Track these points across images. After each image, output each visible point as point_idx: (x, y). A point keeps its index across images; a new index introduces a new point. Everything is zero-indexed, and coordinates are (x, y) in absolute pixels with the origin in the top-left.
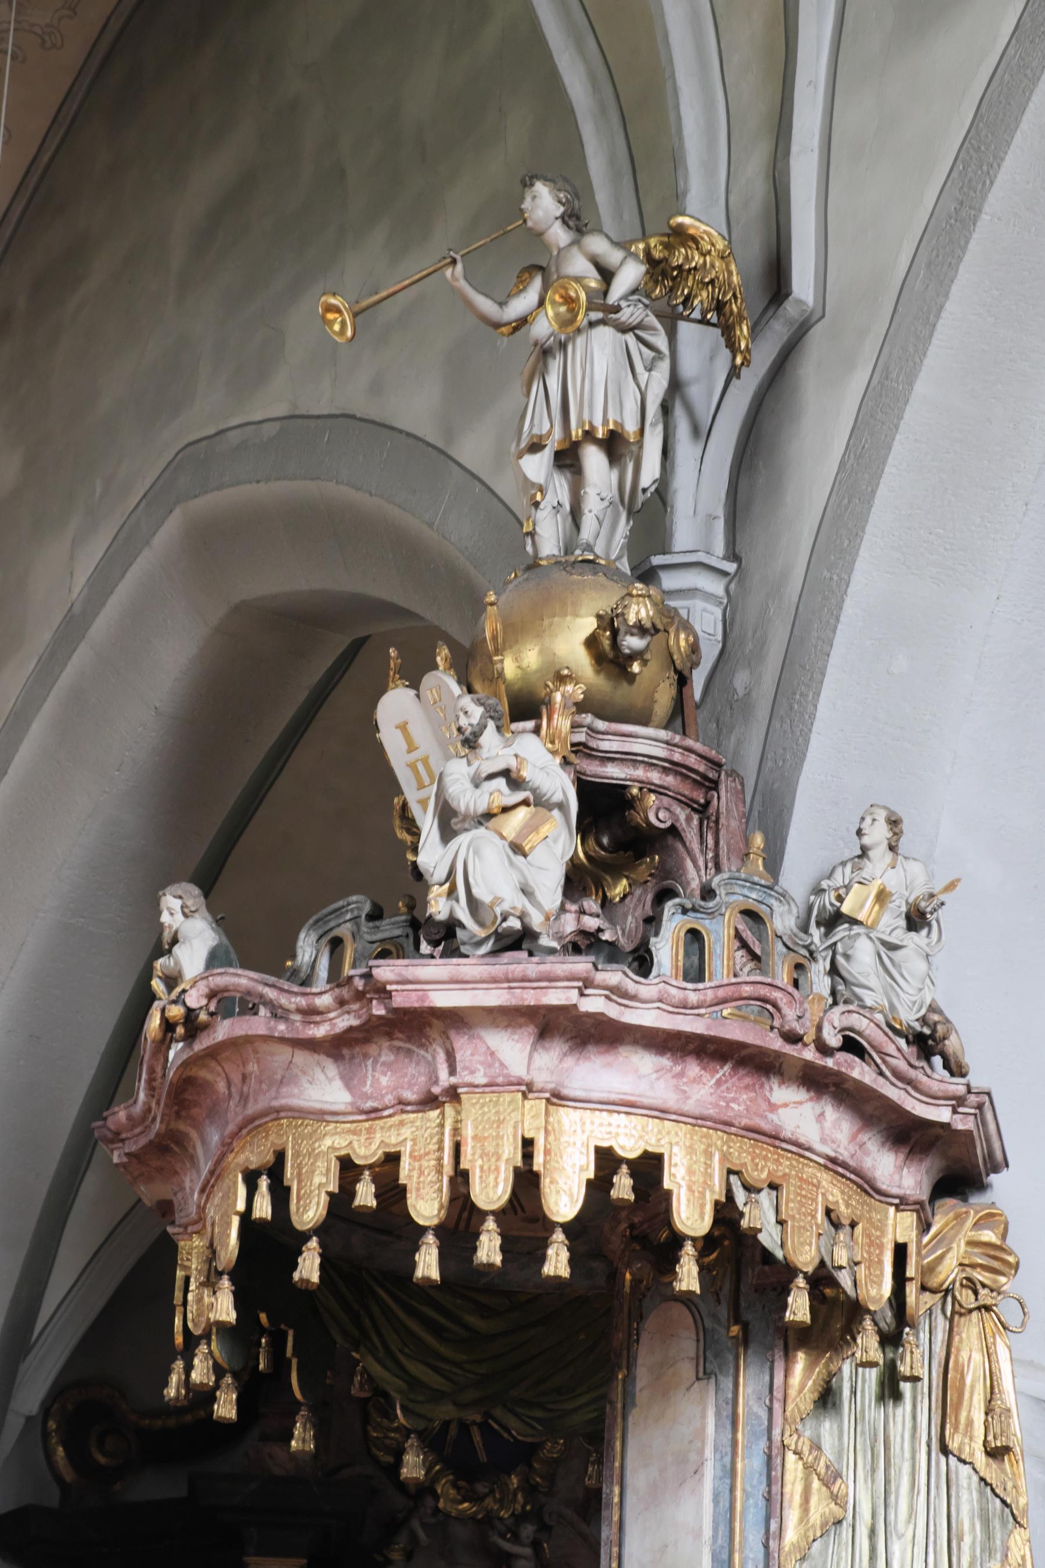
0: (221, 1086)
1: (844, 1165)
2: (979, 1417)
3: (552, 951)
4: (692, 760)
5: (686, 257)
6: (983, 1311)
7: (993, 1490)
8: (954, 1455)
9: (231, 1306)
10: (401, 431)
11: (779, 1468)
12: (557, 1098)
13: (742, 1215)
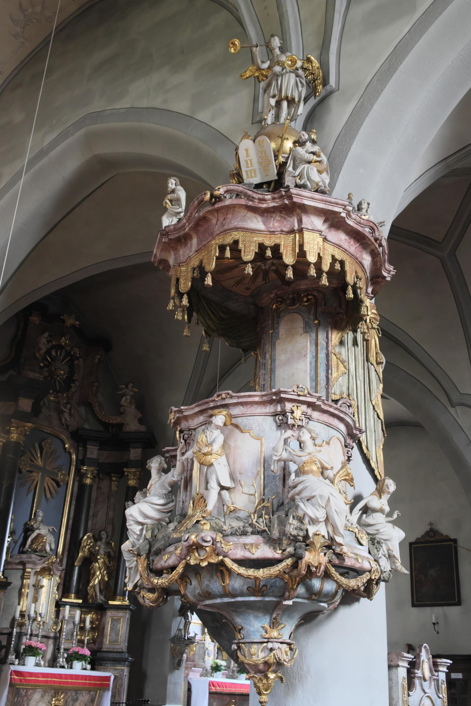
0: (214, 221)
5: (308, 66)
10: (174, 112)
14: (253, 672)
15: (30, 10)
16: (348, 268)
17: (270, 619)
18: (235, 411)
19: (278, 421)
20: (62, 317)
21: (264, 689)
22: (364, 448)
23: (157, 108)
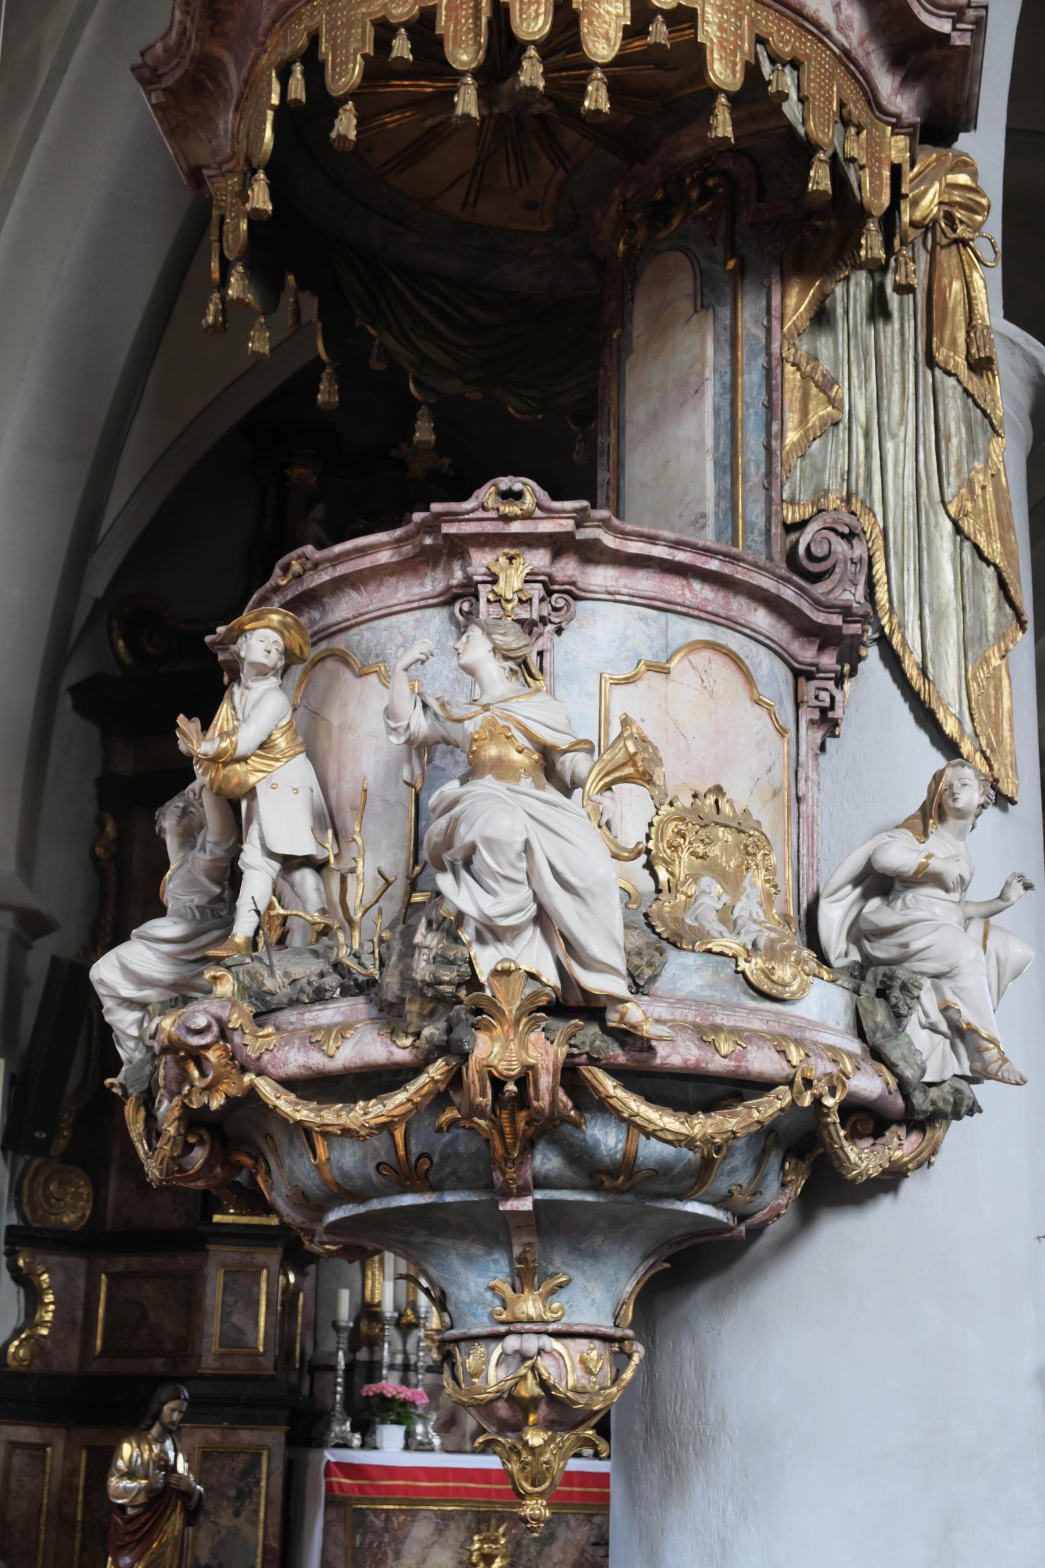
2: (961, 336)
6: (961, 245)
7: (975, 402)
8: (940, 368)
9: (267, 197)
11: (779, 377)
14: (494, 1429)
17: (511, 1264)
19: (461, 618)
20: (394, 453)
21: (526, 1480)
22: (912, 672)
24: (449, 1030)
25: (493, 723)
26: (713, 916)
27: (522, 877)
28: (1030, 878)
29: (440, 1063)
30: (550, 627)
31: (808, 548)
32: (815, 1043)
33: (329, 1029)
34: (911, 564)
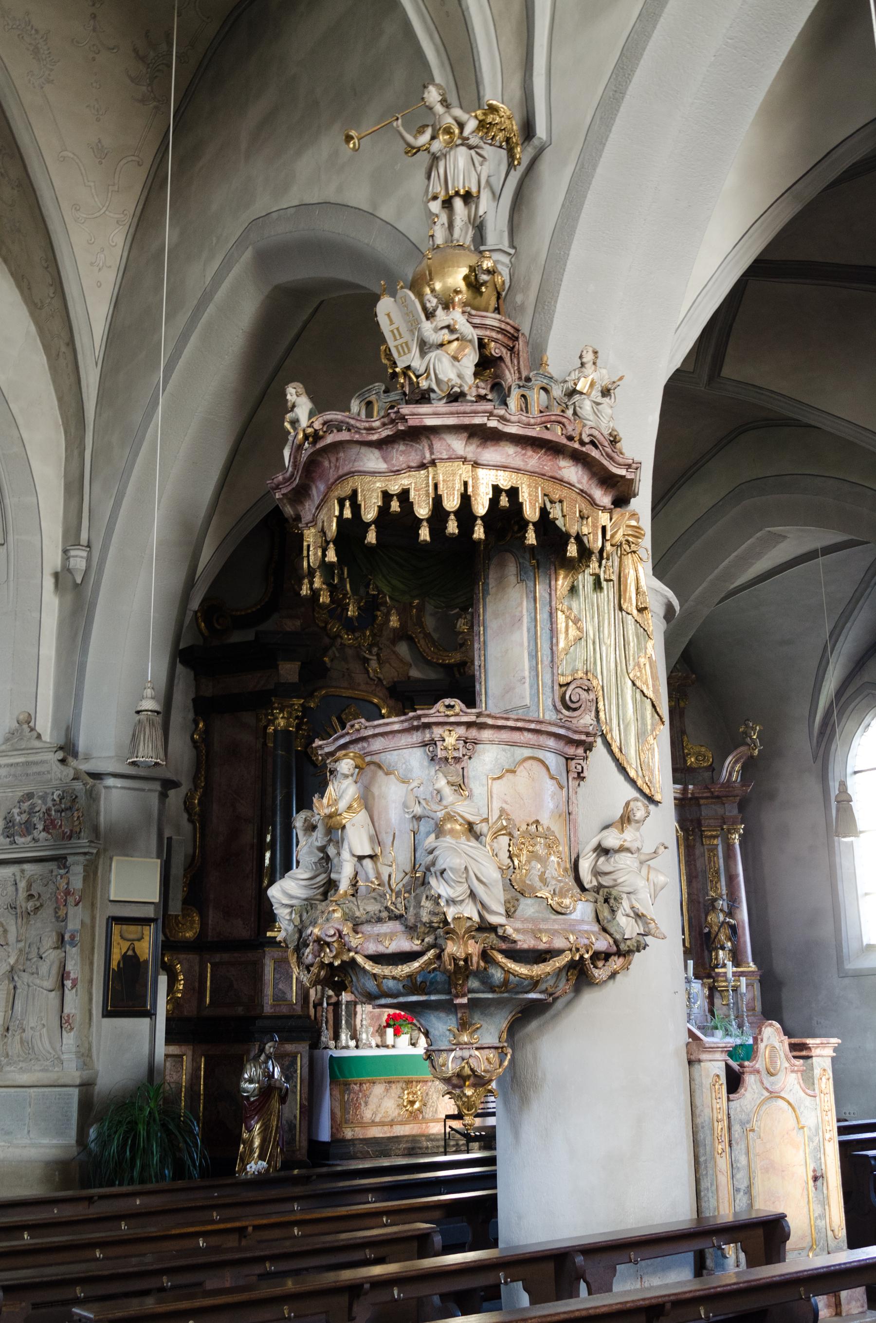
0: (326, 464)
1: (586, 493)
3: (472, 402)
4: (508, 328)
5: (493, 119)
12: (476, 464)
13: (549, 513)
15: (152, 54)
16: (524, 496)
18: (377, 744)
22: (616, 750)
23: (332, 201)
24: (436, 939)
25: (448, 813)
26: (537, 879)
27: (464, 880)
28: (667, 844)
29: (432, 951)
30: (466, 757)
31: (570, 697)
32: (580, 931)
33: (385, 935)
34: (614, 701)
